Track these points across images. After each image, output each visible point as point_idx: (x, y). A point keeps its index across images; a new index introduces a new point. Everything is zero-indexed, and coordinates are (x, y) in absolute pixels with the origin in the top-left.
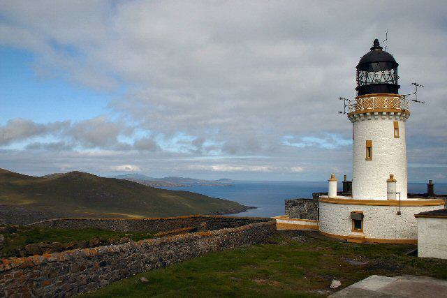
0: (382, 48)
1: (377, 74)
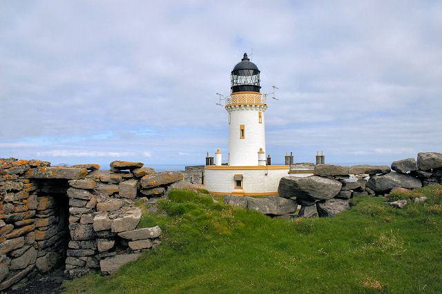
0: (249, 60)
1: (245, 80)
